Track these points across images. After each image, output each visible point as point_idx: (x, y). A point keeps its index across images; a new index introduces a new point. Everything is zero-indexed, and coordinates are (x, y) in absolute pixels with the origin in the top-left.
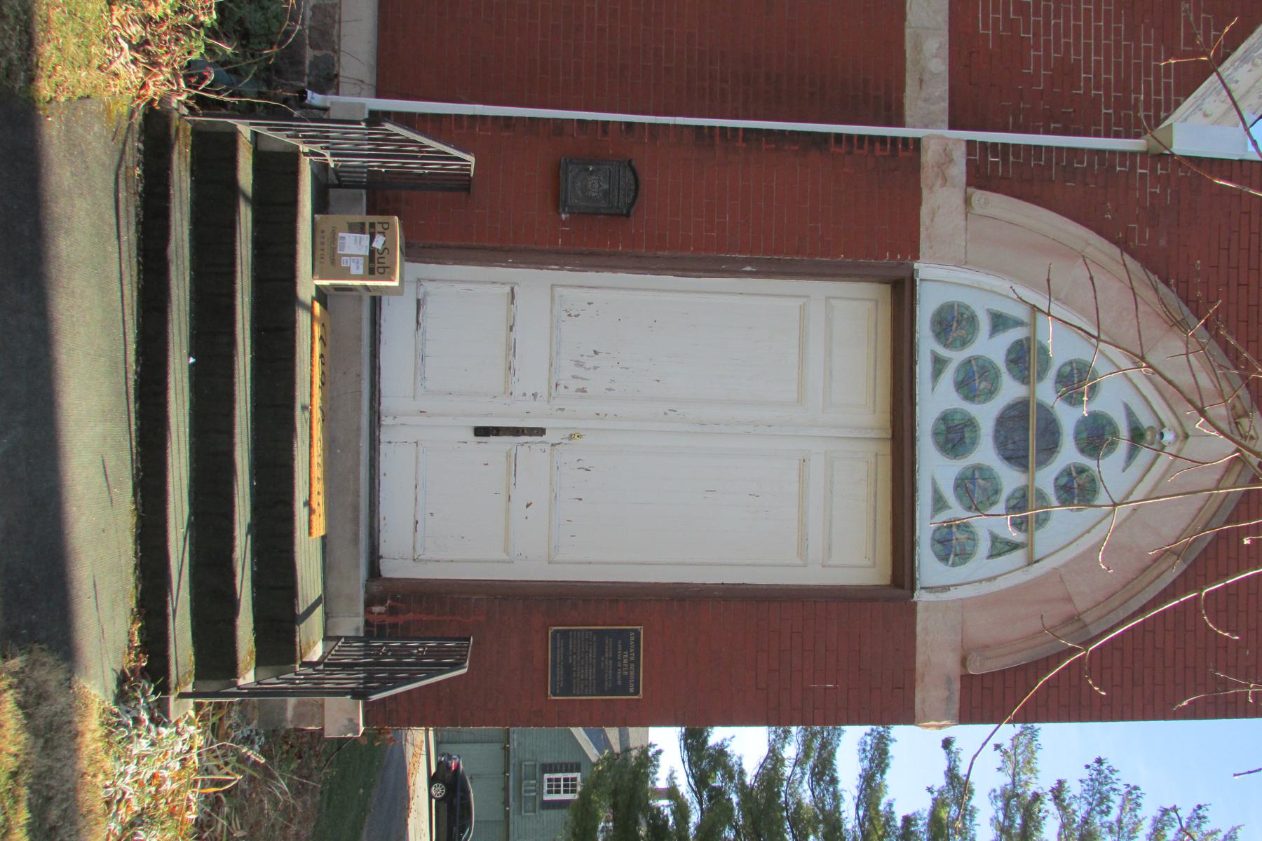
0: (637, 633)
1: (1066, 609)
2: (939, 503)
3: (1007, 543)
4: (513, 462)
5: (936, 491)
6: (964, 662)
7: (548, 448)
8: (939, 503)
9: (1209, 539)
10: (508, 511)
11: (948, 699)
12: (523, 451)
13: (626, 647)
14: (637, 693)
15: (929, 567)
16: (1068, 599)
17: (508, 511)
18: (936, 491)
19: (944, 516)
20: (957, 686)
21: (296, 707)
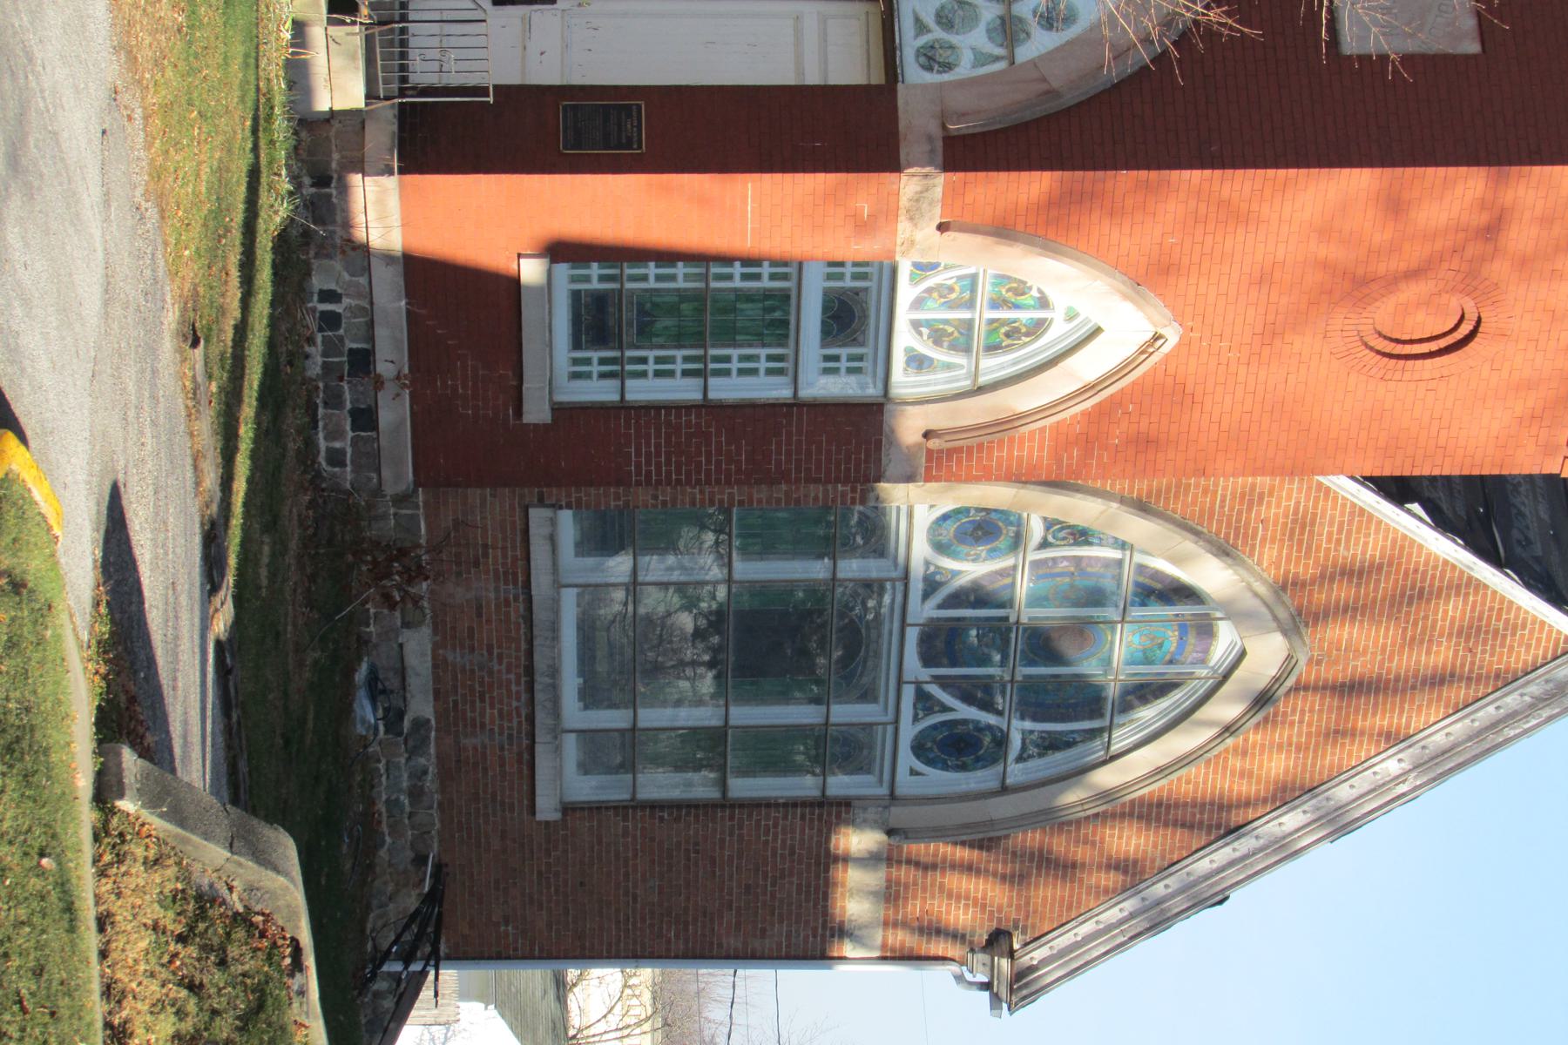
0: (639, 107)
1: (1044, 87)
2: (921, 28)
3: (991, 55)
4: (528, 25)
5: (917, 20)
6: (944, 127)
7: (559, 14)
8: (921, 28)
9: (1369, 548)
10: (523, 58)
11: (932, 151)
12: (536, 17)
13: (629, 116)
14: (640, 147)
15: (913, 73)
16: (1044, 80)
17: (523, 58)
18: (917, 20)
19: (925, 39)
20: (939, 144)
21: (353, 341)
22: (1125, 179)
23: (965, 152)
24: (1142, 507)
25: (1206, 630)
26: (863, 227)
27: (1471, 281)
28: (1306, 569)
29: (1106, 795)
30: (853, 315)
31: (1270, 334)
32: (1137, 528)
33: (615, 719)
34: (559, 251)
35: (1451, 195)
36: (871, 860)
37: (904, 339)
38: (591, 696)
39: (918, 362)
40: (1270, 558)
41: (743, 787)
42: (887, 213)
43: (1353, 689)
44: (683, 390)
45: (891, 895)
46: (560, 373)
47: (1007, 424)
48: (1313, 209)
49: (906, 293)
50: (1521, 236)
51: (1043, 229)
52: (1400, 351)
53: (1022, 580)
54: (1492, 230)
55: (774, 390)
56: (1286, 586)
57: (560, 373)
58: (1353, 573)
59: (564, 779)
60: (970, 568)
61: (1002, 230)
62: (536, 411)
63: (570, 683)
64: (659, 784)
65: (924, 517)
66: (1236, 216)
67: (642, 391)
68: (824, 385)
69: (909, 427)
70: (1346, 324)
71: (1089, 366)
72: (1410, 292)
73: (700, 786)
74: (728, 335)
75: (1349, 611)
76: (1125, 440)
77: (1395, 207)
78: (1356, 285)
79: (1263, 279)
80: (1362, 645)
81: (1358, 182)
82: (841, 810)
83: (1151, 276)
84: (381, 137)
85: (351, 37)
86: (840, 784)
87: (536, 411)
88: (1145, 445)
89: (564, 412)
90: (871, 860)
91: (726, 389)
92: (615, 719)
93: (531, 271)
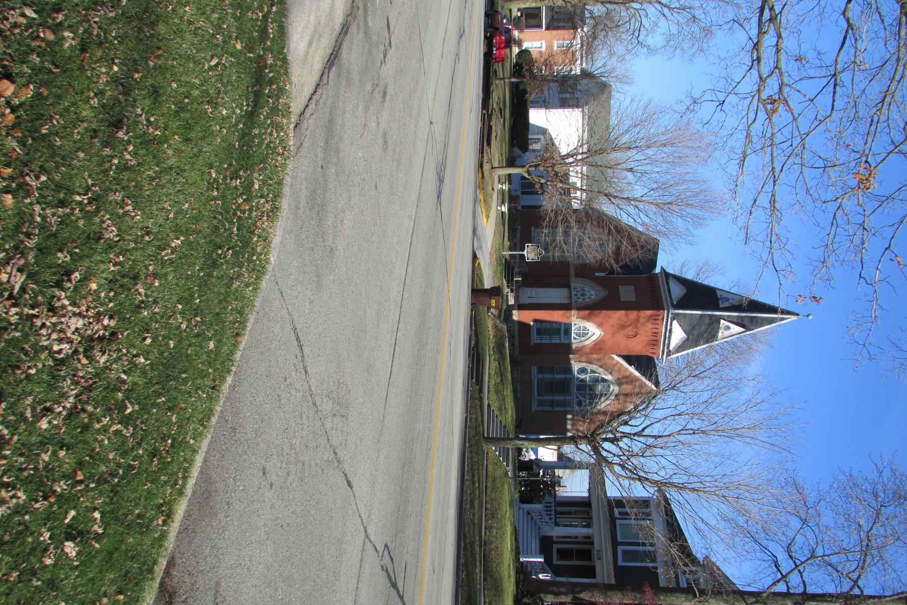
9: (628, 373)
22: (596, 312)
23: (578, 309)
24: (601, 367)
25: (609, 387)
26: (568, 318)
27: (636, 327)
28: (620, 377)
29: (599, 410)
30: (568, 331)
31: (614, 334)
32: (600, 370)
33: (540, 398)
34: (535, 321)
35: (633, 314)
36: (571, 419)
37: (573, 335)
38: (538, 395)
39: (575, 338)
40: (616, 375)
41: (556, 409)
42: (571, 316)
43: (626, 395)
44: (548, 342)
45: (573, 425)
46: (535, 339)
47: (584, 346)
48: (618, 316)
49: (573, 328)
50: (641, 320)
51: (587, 318)
52: (628, 337)
53: (587, 377)
54: (638, 320)
55: (558, 341)
56: (618, 379)
57: (535, 339)
58: (627, 377)
59: (535, 407)
60: (582, 376)
61: (583, 318)
62: (532, 344)
63: (536, 392)
64: (547, 409)
65: (576, 369)
66: (609, 317)
67: (544, 341)
68: (563, 341)
69: (574, 346)
70: (622, 332)
71: (594, 338)
72: (630, 328)
73: (550, 409)
74: (553, 334)
75: (627, 383)
76: (599, 347)
77: (627, 316)
78: (623, 327)
79: (613, 326)
80: (627, 388)
81: (623, 312)
82: (567, 413)
83: (600, 325)
84: (516, 307)
85: (513, 294)
86: (567, 409)
87: (532, 344)
88: (600, 349)
89: (536, 344)
90: (571, 419)
91: (553, 341)
92: (540, 398)
93: (532, 323)
